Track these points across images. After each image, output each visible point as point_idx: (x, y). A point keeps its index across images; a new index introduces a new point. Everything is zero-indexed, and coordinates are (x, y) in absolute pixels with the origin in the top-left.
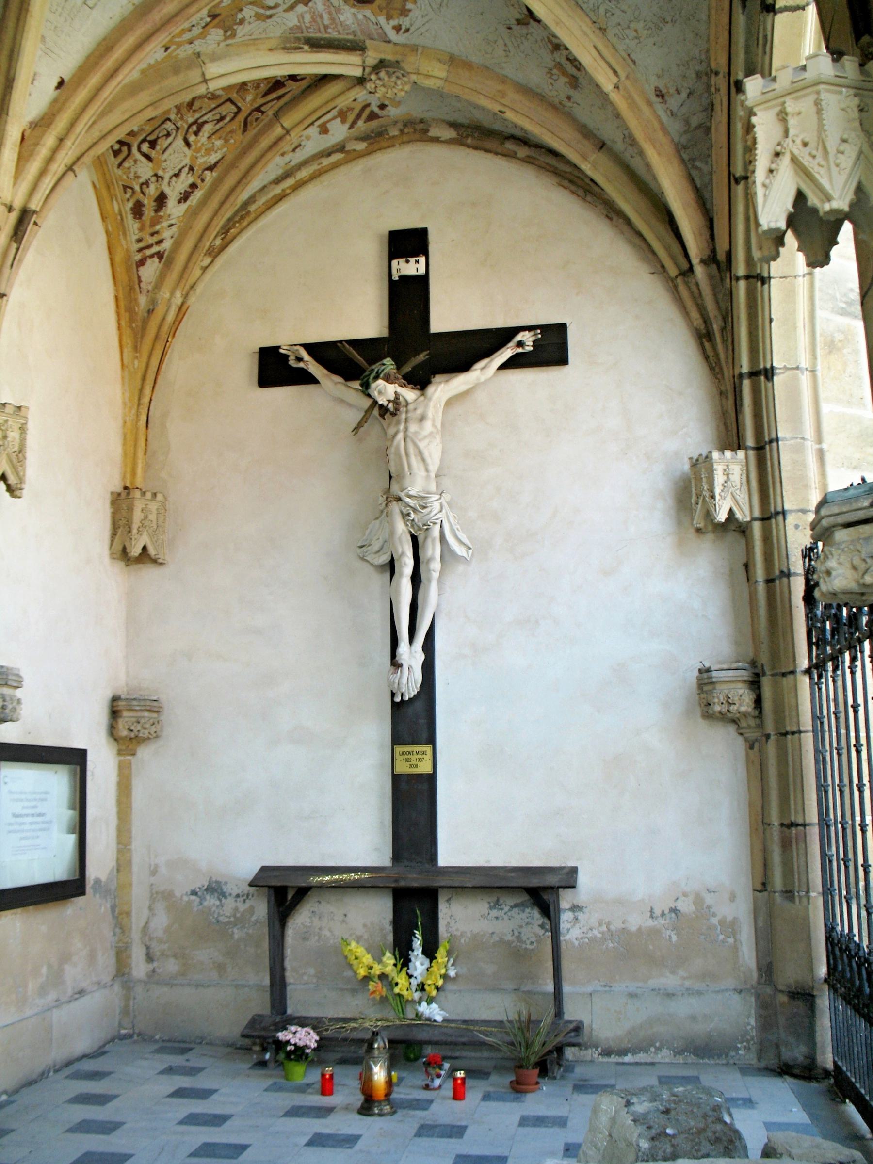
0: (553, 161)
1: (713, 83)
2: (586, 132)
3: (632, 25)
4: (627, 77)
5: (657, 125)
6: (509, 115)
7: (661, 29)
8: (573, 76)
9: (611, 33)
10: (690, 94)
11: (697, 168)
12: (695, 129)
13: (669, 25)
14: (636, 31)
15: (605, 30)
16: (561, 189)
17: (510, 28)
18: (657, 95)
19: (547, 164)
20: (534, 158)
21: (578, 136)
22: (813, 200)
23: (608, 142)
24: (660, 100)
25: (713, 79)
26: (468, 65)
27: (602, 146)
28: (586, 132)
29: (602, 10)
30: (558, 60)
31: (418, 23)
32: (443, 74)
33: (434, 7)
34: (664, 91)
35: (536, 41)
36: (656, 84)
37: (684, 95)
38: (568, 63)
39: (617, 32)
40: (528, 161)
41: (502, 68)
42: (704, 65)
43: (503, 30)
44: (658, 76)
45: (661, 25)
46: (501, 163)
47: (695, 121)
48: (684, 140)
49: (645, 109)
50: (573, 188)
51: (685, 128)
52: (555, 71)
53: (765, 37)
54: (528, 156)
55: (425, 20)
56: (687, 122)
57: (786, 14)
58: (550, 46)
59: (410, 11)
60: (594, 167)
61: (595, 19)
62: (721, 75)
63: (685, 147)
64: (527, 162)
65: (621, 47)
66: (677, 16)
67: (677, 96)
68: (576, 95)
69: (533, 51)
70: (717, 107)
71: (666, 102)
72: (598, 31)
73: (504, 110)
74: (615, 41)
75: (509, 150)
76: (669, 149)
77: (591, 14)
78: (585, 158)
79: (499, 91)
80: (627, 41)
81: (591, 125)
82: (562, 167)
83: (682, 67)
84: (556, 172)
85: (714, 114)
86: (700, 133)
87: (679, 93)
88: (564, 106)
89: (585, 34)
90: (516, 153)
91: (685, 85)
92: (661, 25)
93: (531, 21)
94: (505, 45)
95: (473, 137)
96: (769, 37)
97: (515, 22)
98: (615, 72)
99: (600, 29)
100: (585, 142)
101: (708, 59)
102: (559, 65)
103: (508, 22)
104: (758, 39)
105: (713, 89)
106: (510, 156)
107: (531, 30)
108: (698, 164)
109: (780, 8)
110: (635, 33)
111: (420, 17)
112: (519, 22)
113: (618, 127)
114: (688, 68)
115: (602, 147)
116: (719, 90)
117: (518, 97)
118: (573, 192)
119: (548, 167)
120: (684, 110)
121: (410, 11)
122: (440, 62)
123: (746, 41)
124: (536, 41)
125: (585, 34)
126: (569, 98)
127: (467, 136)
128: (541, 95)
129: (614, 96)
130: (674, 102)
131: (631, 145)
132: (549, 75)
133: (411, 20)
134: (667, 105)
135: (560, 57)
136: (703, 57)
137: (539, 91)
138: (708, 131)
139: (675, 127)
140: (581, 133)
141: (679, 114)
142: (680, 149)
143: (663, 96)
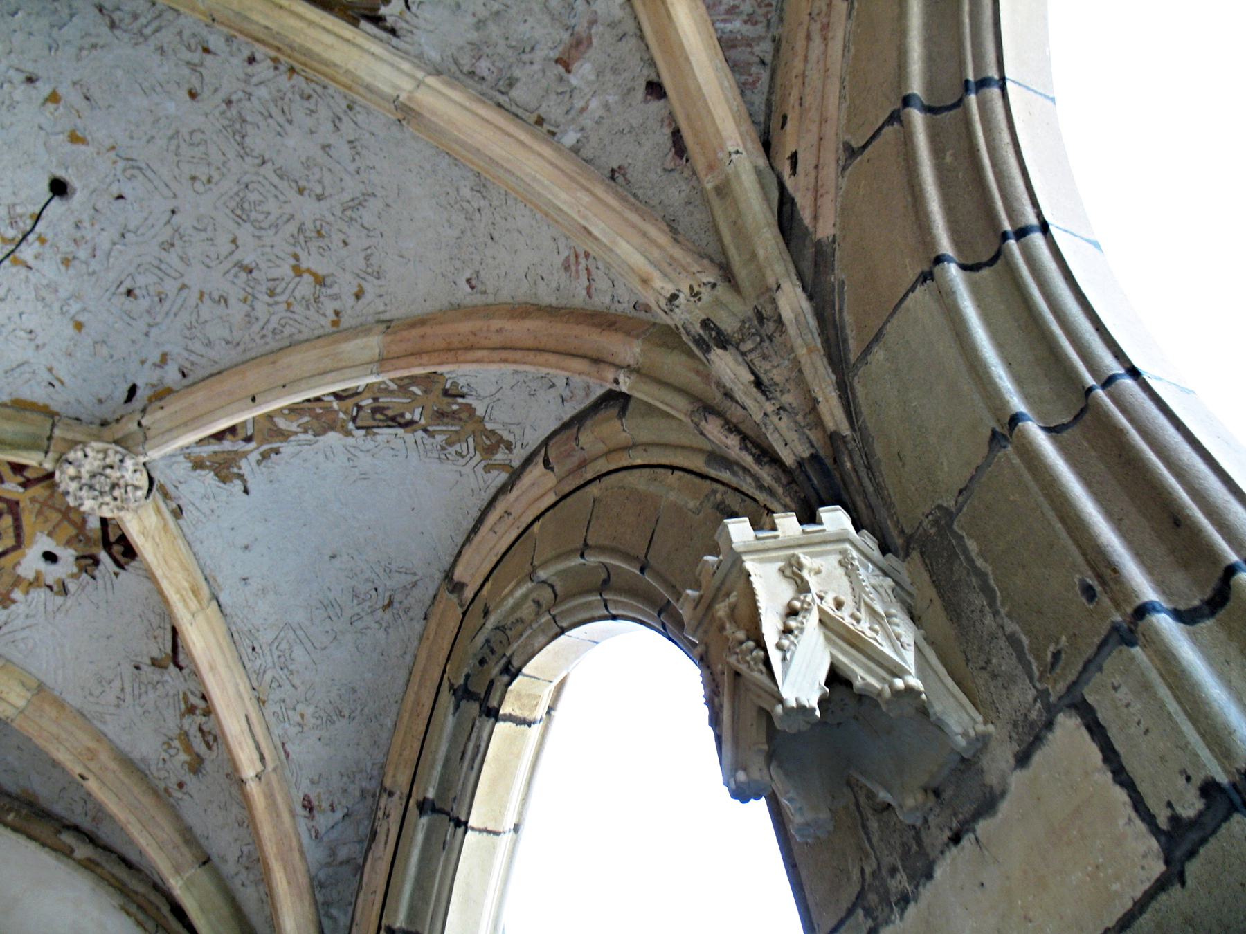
0: (122, 873)
1: (382, 805)
2: (189, 837)
3: (300, 707)
4: (275, 770)
5: (295, 843)
6: (92, 785)
7: (333, 722)
8: (198, 755)
9: (270, 708)
10: (346, 815)
11: (331, 917)
12: (341, 863)
13: (345, 721)
14: (302, 716)
15: (264, 702)
16: (124, 915)
17: (137, 668)
18: (304, 807)
19: (113, 875)
20: (98, 864)
21: (179, 840)
22: (863, 676)
23: (215, 859)
24: (306, 813)
25: (384, 800)
26: (60, 704)
27: (206, 861)
28: (189, 837)
29: (268, 677)
30: (186, 727)
31: (19, 623)
32: (21, 703)
33: (50, 608)
34: (315, 803)
35: (167, 695)
36: (307, 792)
37: (339, 815)
38: (199, 734)
39: (278, 710)
40: (88, 865)
41: (105, 723)
42: (374, 783)
43: (127, 669)
44: (312, 782)
45: (335, 718)
46: (46, 859)
47: (343, 853)
48: (322, 875)
49: (286, 817)
50: (141, 917)
51: (329, 860)
52: (176, 743)
53: (477, 747)
54: (89, 860)
55: (29, 622)
56: (333, 853)
57: (509, 724)
58: (183, 706)
59: (14, 602)
60: (189, 885)
61: (255, 685)
62: (396, 797)
63: (321, 885)
64: (86, 867)
65: (277, 731)
66: (358, 712)
67: (330, 813)
68: (191, 782)
69: (157, 708)
70: (381, 837)
71: (312, 818)
72: (255, 701)
73: (86, 774)
74: (272, 720)
75: (64, 843)
76: (303, 880)
77: (254, 677)
78: (178, 870)
79: (89, 749)
80: (287, 725)
81: (198, 830)
82: (134, 884)
83: (345, 779)
84: (122, 889)
85: (373, 846)
86: (346, 870)
87: (333, 810)
88: (170, 795)
89: (241, 696)
90: (72, 851)
91: (344, 802)
92: (335, 718)
93: (171, 666)
94: (122, 690)
95: (18, 813)
96: (482, 749)
97: (149, 662)
98: (262, 758)
99: (258, 699)
100: (185, 850)
101: (383, 776)
102: (184, 736)
103: (139, 659)
104: (463, 753)
105: (380, 814)
106: (66, 853)
107: (166, 678)
108: (334, 912)
109: (504, 715)
110: (298, 719)
111: (22, 616)
112: (154, 662)
113: (236, 840)
114: (353, 782)
115: (204, 863)
116: (388, 816)
117: (113, 765)
118: (139, 924)
119: (112, 881)
120: (334, 834)
121: (14, 602)
122: (24, 685)
123: (448, 751)
124: (167, 695)
125: (241, 696)
126: (181, 785)
127: (9, 810)
128: (142, 772)
129: (253, 788)
130: (323, 821)
131: (247, 868)
132: (165, 747)
133: (9, 616)
134: (314, 823)
135: (191, 724)
136: (375, 773)
137: (142, 766)
138: (360, 869)
139: (317, 854)
140: (183, 835)
141: (325, 839)
142: (316, 884)
143: (311, 810)
